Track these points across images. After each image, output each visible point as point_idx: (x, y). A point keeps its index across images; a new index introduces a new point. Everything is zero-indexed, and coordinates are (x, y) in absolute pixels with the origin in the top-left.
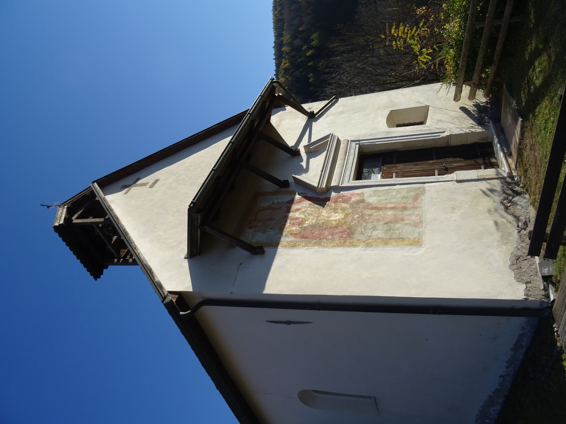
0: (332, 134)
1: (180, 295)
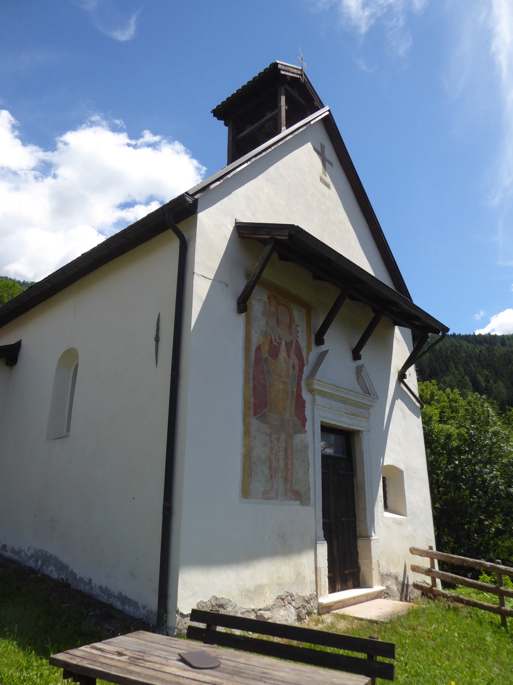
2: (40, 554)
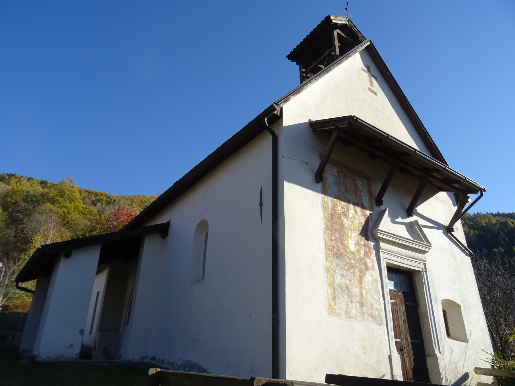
0: (431, 246)
1: (279, 118)
2: (187, 363)
